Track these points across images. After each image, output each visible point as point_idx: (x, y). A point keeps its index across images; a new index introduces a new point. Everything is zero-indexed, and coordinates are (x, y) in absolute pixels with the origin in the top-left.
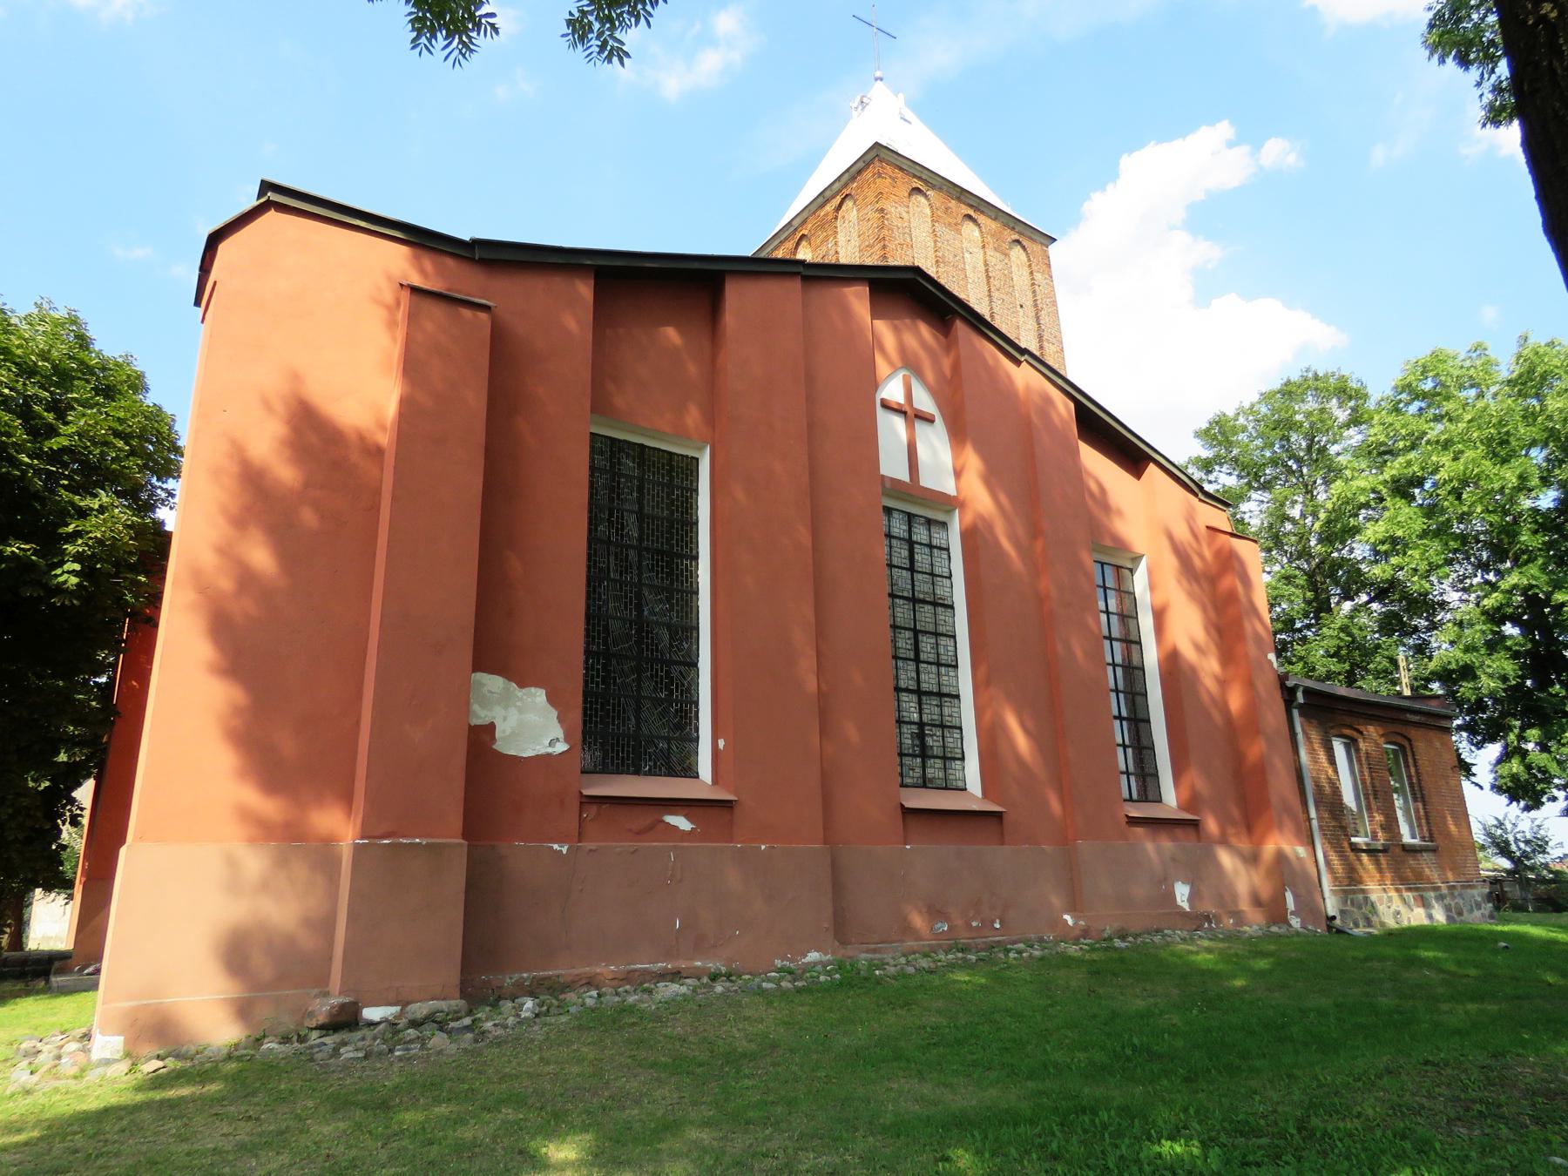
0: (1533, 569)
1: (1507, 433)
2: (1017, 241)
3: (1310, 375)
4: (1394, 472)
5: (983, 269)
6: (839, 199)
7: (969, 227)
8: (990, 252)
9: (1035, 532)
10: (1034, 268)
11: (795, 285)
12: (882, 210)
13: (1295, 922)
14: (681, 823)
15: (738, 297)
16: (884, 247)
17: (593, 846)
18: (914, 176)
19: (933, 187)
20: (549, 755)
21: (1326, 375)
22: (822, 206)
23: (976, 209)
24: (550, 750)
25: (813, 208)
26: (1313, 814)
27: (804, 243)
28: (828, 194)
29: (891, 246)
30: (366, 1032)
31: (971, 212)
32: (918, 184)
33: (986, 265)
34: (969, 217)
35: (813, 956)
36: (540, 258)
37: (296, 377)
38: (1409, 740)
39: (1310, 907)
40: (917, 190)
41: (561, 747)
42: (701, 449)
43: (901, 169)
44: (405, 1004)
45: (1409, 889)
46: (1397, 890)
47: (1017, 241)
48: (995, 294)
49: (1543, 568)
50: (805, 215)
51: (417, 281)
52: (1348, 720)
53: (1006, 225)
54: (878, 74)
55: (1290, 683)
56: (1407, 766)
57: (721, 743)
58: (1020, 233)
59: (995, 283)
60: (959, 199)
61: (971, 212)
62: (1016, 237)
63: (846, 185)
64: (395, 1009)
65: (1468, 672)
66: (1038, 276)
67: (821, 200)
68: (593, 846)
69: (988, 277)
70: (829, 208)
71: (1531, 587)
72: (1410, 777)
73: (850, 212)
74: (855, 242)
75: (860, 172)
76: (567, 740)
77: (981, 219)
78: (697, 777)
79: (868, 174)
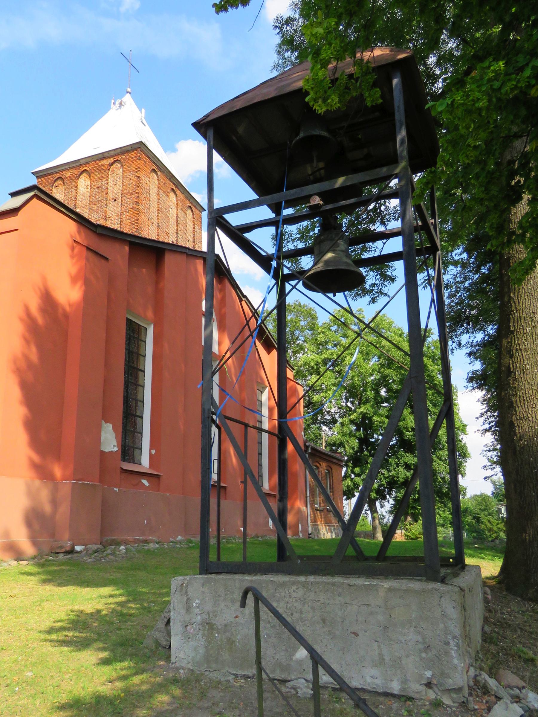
0: (368, 406)
1: (369, 350)
2: (190, 207)
3: (297, 303)
4: (326, 356)
5: (175, 218)
6: (112, 160)
7: (172, 195)
8: (180, 211)
9: (243, 373)
10: (196, 222)
11: (184, 257)
12: (139, 177)
13: (301, 535)
14: (145, 482)
15: (169, 259)
16: (138, 197)
17: (125, 490)
18: (154, 163)
19: (160, 170)
20: (112, 451)
21: (304, 306)
22: (101, 159)
23: (176, 187)
24: (113, 450)
25: (95, 158)
26: (308, 495)
27: (85, 174)
28: (106, 155)
29: (141, 198)
30: (76, 555)
31: (174, 188)
32: (154, 167)
33: (177, 216)
34: (173, 189)
35: (179, 538)
36: (118, 236)
37: (44, 279)
38: (332, 469)
39: (305, 529)
40: (154, 170)
41: (116, 449)
42: (149, 324)
43: (149, 158)
44: (85, 545)
45: (328, 526)
46: (325, 526)
47: (190, 207)
48: (179, 232)
49: (372, 406)
50: (90, 160)
51: (78, 239)
52: (318, 460)
53: (187, 198)
54: (129, 90)
55: (307, 444)
56: (330, 479)
57: (153, 452)
58: (192, 203)
59: (180, 226)
60: (170, 179)
61: (174, 188)
62: (190, 205)
63: (118, 155)
64: (83, 547)
65: (341, 445)
66: (196, 227)
67: (101, 156)
68: (125, 490)
69: (177, 223)
70: (105, 162)
71: (367, 413)
72: (330, 483)
73: (118, 170)
74: (119, 187)
75: (128, 151)
76: (118, 447)
77: (178, 192)
78: (141, 464)
79: (133, 154)
